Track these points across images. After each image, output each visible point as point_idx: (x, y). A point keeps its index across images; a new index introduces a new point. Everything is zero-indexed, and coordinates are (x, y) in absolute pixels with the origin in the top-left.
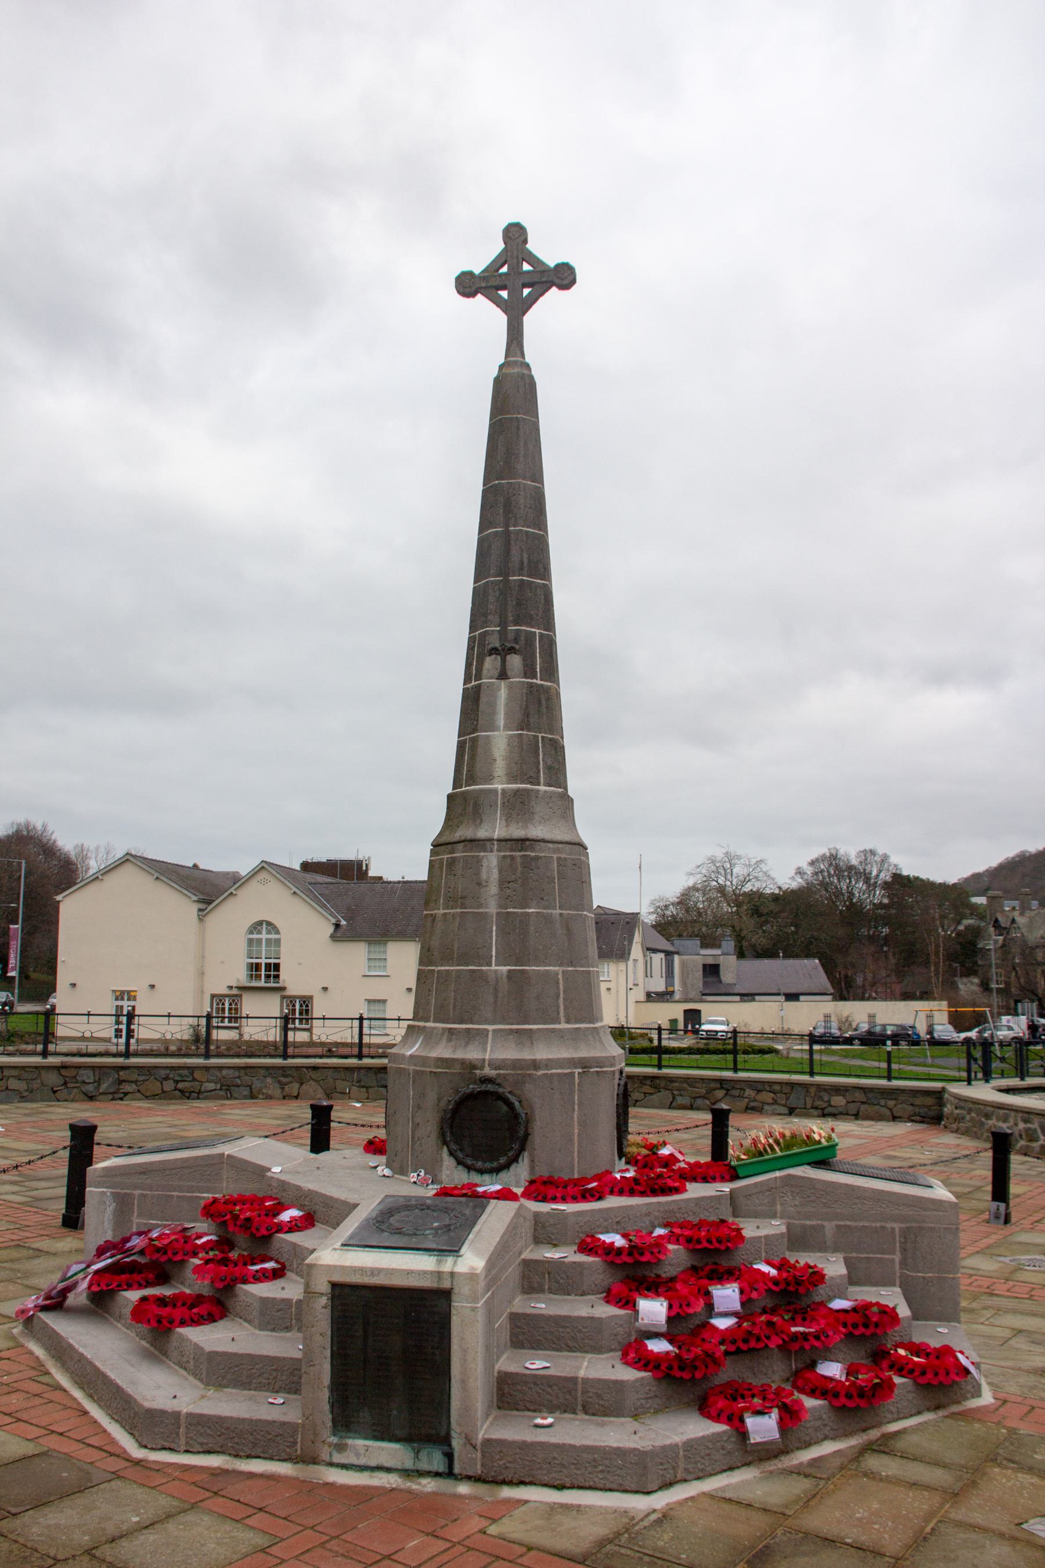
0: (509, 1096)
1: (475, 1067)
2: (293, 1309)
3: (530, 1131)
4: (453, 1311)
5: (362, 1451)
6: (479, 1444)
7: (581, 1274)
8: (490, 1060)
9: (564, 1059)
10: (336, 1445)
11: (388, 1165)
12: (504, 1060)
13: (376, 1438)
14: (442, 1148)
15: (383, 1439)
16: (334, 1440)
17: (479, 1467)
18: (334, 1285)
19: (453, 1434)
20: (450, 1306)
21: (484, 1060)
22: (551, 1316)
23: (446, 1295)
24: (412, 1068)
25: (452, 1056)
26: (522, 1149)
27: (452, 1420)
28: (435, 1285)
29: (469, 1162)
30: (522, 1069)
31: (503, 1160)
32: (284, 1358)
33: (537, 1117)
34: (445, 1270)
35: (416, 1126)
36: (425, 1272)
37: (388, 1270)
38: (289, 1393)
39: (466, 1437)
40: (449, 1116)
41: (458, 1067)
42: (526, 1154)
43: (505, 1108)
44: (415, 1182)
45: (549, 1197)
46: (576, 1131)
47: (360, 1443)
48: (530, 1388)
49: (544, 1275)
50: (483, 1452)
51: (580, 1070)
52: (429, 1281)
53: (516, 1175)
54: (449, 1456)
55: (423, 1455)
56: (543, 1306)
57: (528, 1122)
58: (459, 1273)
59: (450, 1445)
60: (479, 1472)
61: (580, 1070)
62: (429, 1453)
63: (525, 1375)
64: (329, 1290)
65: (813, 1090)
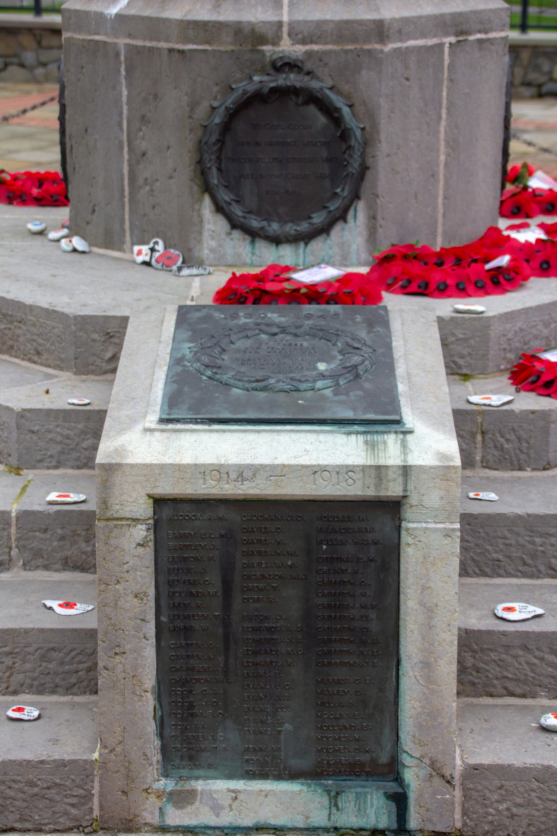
0: (333, 97)
1: (262, 39)
2: (13, 530)
3: (369, 162)
4: (405, 538)
5: (226, 802)
6: (457, 775)
7: (546, 431)
8: (291, 24)
9: (428, 18)
10: (171, 794)
11: (74, 228)
12: (320, 24)
13: (250, 775)
14: (200, 200)
15: (263, 776)
16: (167, 784)
17: (458, 815)
18: (159, 502)
19: (406, 760)
20: (399, 528)
21: (280, 24)
22: (519, 517)
23: (391, 509)
24: (122, 42)
25: (214, 17)
26: (356, 196)
27: (402, 735)
28: (371, 493)
29: (255, 223)
30: (354, 39)
31: (318, 218)
32: (27, 631)
33: (383, 136)
34: (390, 462)
35: (139, 157)
36: (350, 469)
37: (273, 467)
38: (40, 692)
39: (433, 764)
40: (214, 137)
41: (229, 39)
42: (361, 206)
43: (322, 119)
44: (147, 264)
45: (432, 286)
46: (442, 158)
47: (221, 786)
48: (515, 657)
49: (473, 435)
50: (465, 790)
51: (453, 39)
52: (359, 483)
53: (342, 245)
54: (400, 801)
55: (348, 801)
56: (492, 496)
57: (366, 143)
58: (420, 467)
59: (399, 779)
60: (459, 825)
61: (453, 39)
62: (358, 796)
63: (504, 634)
64: (150, 512)
65: (525, 55)
